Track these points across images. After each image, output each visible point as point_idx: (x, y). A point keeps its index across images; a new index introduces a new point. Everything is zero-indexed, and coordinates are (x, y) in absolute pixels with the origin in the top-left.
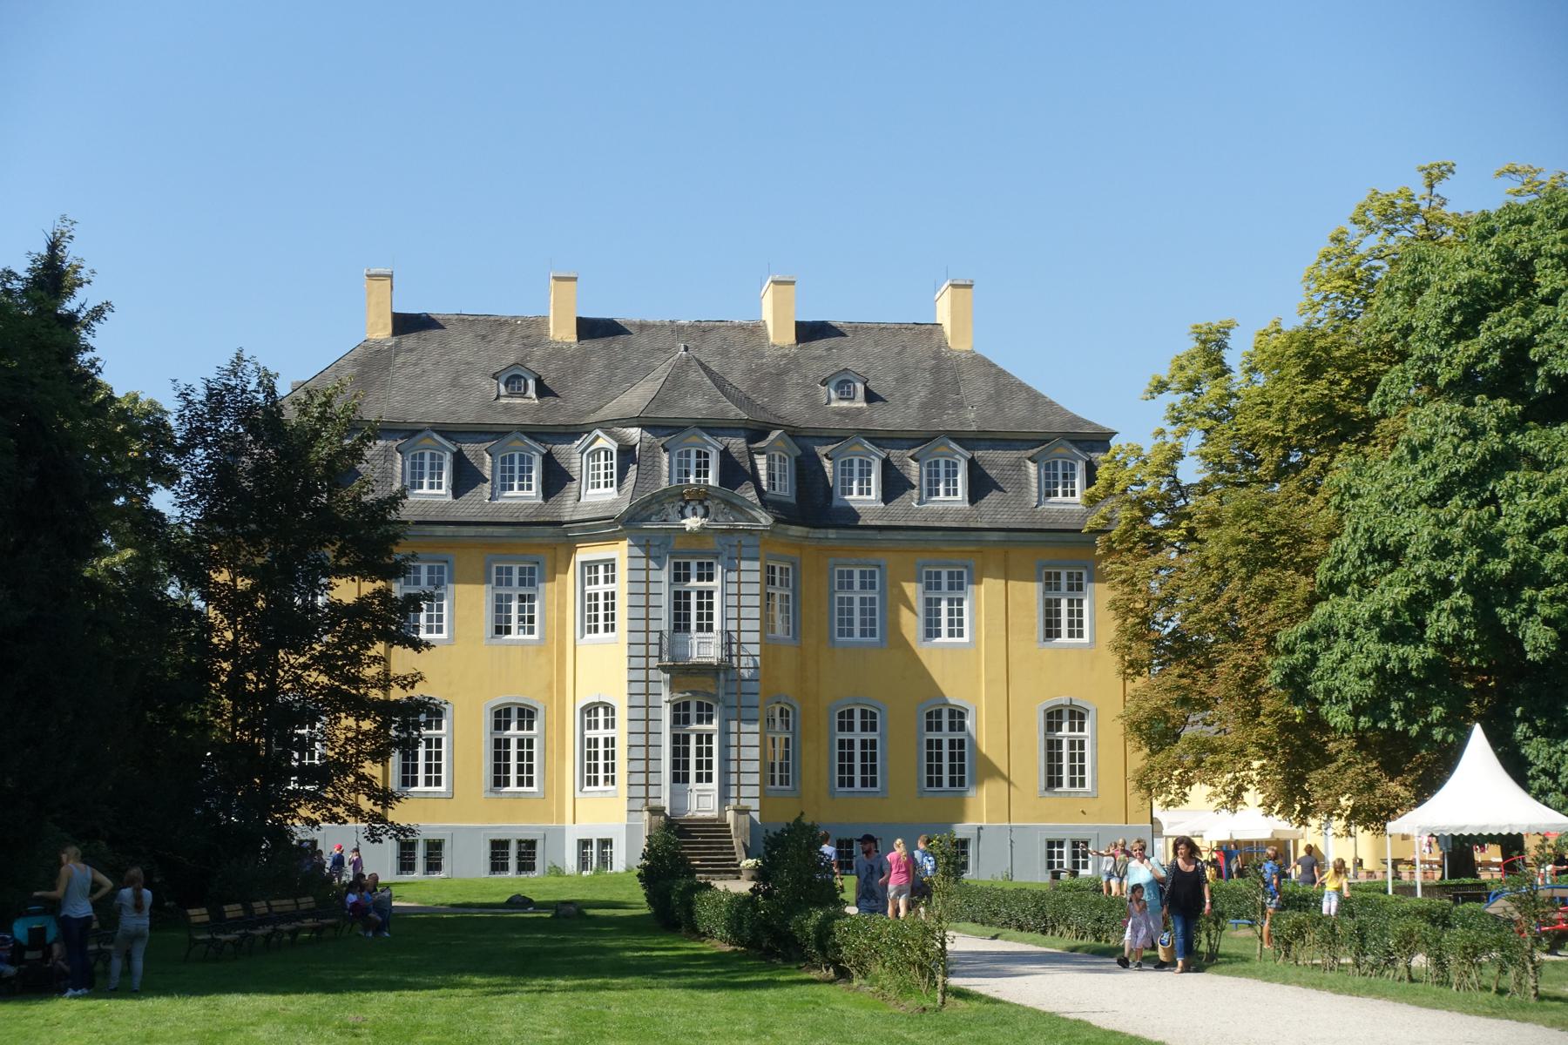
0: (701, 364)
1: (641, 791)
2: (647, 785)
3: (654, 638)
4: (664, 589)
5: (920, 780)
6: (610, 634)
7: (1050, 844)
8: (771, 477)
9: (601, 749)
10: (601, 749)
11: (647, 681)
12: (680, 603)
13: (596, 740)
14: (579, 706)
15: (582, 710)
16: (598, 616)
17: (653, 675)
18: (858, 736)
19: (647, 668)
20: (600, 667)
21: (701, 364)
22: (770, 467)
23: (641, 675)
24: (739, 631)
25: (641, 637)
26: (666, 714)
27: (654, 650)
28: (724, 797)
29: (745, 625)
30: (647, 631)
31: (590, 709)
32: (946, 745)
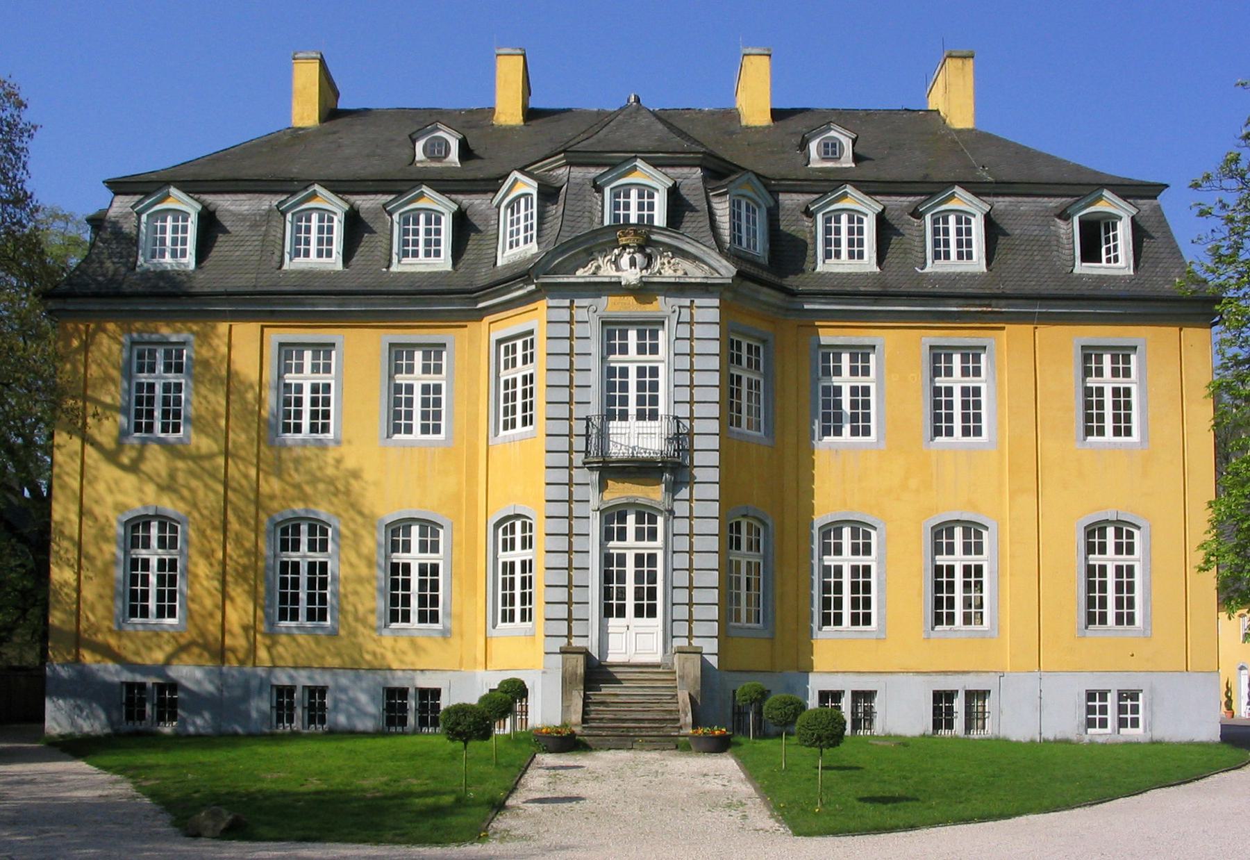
0: (872, 800)
1: (562, 628)
2: (569, 620)
3: (579, 427)
4: (594, 363)
5: (1150, 705)
6: (529, 428)
7: (1091, 696)
8: (735, 227)
9: (518, 576)
10: (518, 576)
11: (570, 484)
12: (613, 380)
13: (512, 564)
14: (494, 519)
15: (497, 526)
16: (514, 407)
17: (579, 476)
18: (958, 560)
19: (570, 467)
20: (520, 469)
21: (872, 800)
22: (735, 216)
23: (563, 476)
24: (691, 418)
25: (563, 443)
26: (594, 527)
27: (579, 444)
28: (668, 636)
29: (699, 410)
30: (570, 452)
31: (506, 523)
32: (1111, 572)
